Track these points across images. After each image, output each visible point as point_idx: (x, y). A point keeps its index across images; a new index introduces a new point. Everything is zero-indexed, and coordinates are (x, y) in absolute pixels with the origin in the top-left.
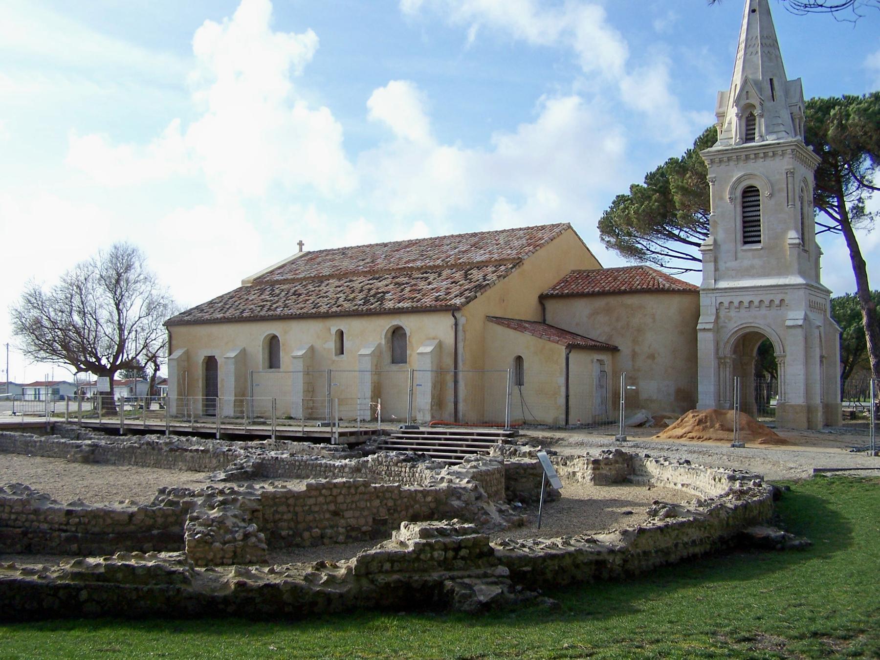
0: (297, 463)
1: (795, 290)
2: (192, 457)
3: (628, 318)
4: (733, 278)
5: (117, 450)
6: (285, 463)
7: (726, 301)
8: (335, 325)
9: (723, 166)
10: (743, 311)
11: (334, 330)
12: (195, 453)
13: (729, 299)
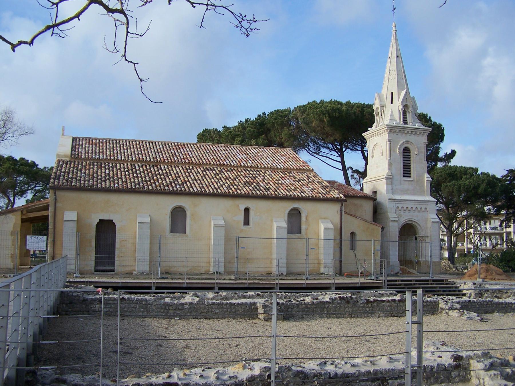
0: (485, 303)
1: (432, 204)
2: (390, 306)
3: (355, 211)
4: (399, 194)
5: (304, 306)
6: (476, 304)
7: (400, 206)
8: (243, 204)
9: (395, 134)
10: (407, 212)
11: (242, 208)
12: (393, 303)
13: (402, 205)
